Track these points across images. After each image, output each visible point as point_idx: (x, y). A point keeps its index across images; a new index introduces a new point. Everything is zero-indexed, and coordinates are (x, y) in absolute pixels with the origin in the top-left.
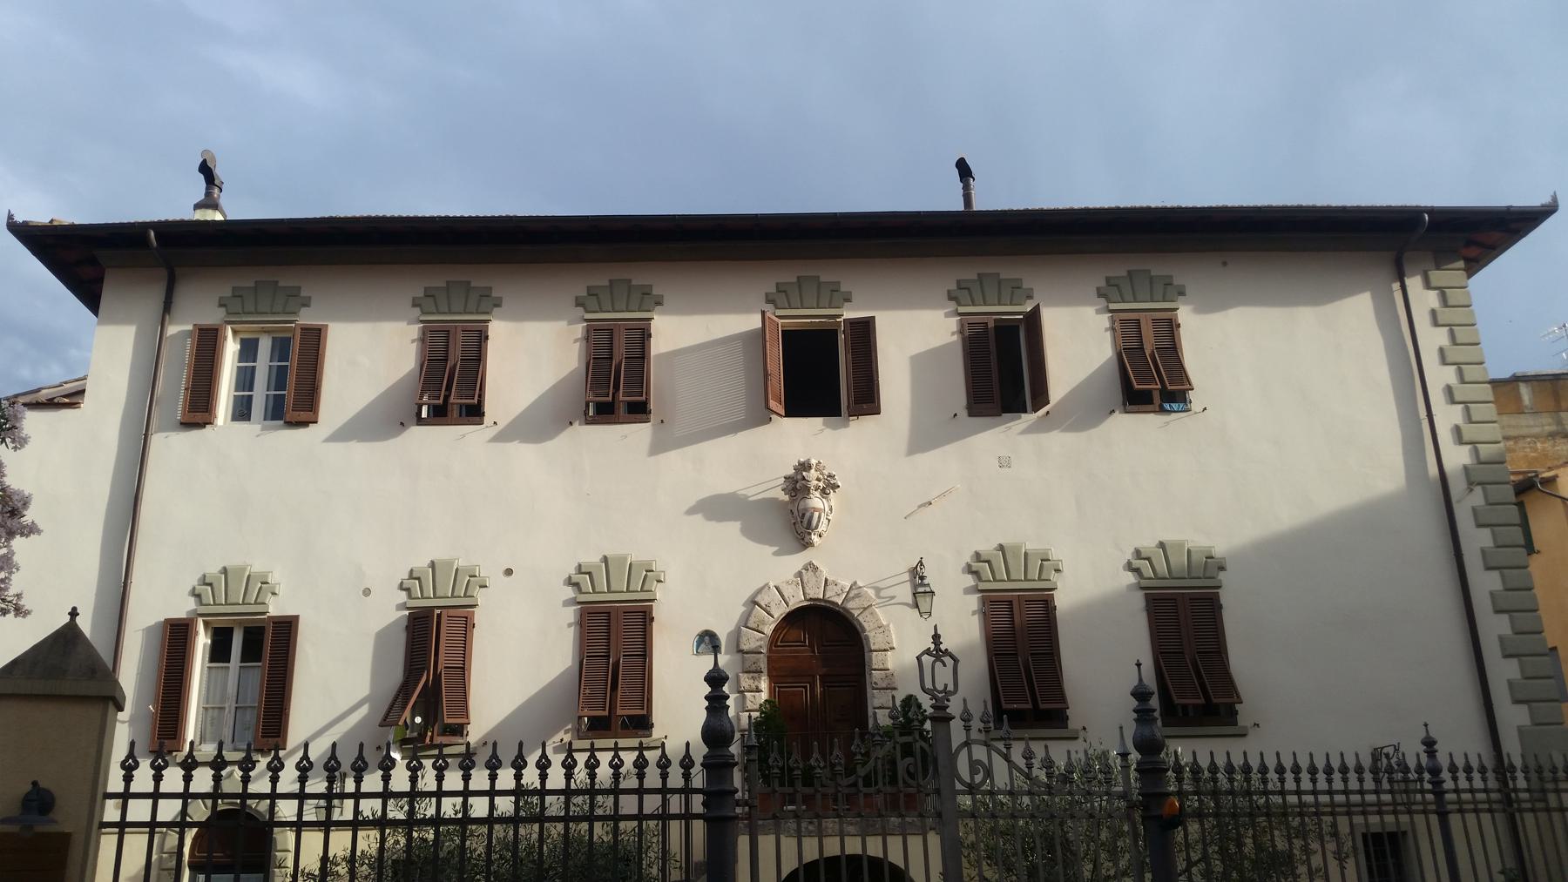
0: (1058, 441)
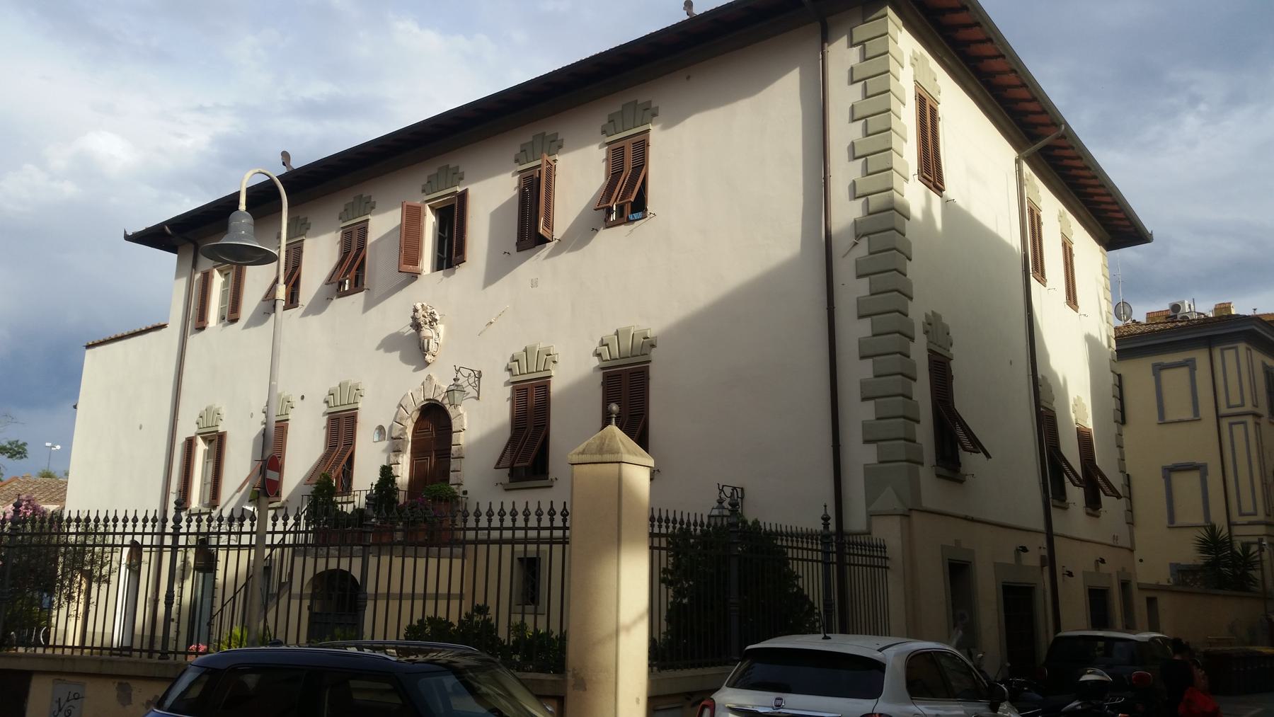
0: (567, 258)
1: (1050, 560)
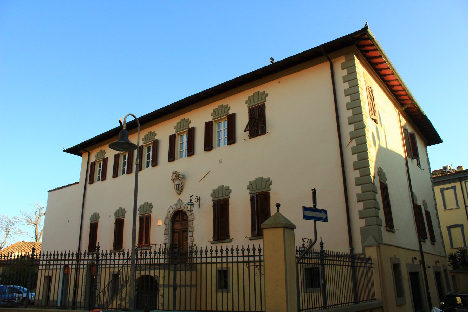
1: (422, 262)
